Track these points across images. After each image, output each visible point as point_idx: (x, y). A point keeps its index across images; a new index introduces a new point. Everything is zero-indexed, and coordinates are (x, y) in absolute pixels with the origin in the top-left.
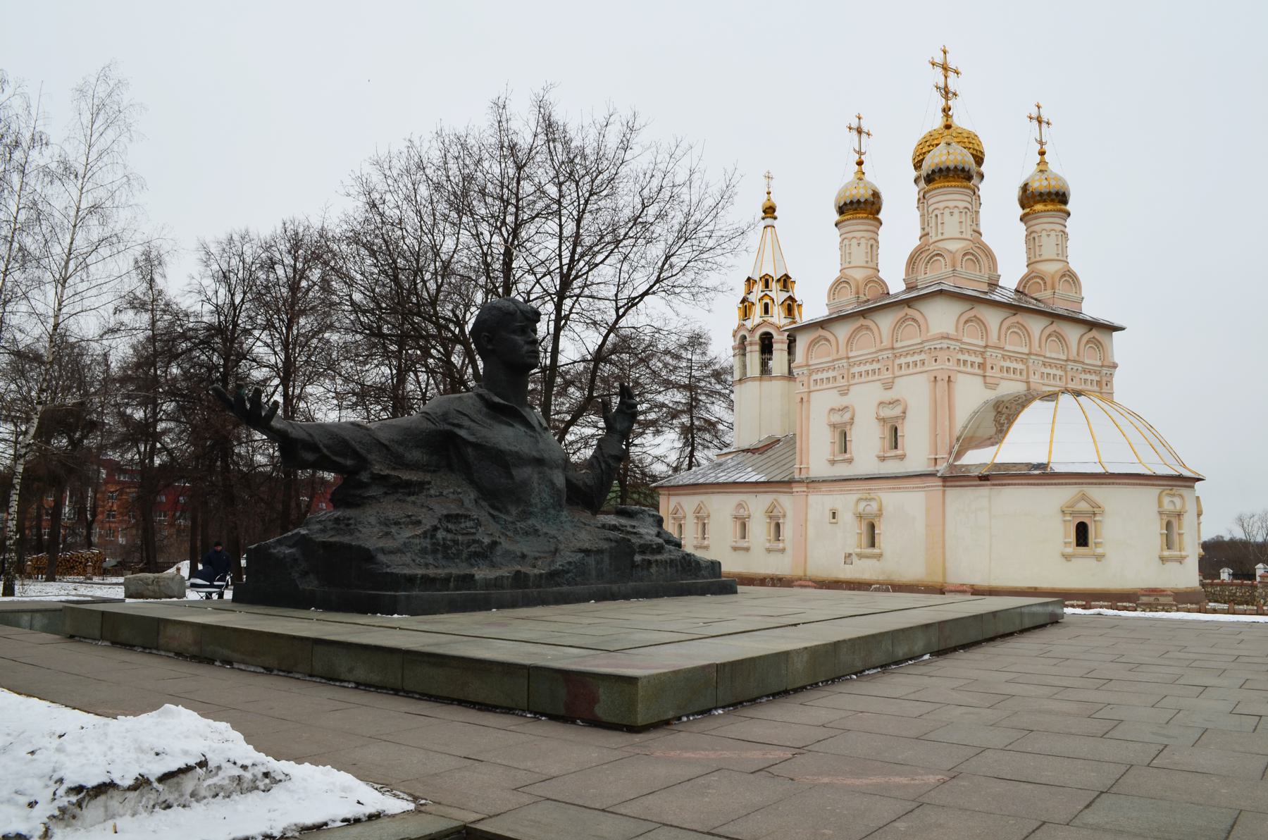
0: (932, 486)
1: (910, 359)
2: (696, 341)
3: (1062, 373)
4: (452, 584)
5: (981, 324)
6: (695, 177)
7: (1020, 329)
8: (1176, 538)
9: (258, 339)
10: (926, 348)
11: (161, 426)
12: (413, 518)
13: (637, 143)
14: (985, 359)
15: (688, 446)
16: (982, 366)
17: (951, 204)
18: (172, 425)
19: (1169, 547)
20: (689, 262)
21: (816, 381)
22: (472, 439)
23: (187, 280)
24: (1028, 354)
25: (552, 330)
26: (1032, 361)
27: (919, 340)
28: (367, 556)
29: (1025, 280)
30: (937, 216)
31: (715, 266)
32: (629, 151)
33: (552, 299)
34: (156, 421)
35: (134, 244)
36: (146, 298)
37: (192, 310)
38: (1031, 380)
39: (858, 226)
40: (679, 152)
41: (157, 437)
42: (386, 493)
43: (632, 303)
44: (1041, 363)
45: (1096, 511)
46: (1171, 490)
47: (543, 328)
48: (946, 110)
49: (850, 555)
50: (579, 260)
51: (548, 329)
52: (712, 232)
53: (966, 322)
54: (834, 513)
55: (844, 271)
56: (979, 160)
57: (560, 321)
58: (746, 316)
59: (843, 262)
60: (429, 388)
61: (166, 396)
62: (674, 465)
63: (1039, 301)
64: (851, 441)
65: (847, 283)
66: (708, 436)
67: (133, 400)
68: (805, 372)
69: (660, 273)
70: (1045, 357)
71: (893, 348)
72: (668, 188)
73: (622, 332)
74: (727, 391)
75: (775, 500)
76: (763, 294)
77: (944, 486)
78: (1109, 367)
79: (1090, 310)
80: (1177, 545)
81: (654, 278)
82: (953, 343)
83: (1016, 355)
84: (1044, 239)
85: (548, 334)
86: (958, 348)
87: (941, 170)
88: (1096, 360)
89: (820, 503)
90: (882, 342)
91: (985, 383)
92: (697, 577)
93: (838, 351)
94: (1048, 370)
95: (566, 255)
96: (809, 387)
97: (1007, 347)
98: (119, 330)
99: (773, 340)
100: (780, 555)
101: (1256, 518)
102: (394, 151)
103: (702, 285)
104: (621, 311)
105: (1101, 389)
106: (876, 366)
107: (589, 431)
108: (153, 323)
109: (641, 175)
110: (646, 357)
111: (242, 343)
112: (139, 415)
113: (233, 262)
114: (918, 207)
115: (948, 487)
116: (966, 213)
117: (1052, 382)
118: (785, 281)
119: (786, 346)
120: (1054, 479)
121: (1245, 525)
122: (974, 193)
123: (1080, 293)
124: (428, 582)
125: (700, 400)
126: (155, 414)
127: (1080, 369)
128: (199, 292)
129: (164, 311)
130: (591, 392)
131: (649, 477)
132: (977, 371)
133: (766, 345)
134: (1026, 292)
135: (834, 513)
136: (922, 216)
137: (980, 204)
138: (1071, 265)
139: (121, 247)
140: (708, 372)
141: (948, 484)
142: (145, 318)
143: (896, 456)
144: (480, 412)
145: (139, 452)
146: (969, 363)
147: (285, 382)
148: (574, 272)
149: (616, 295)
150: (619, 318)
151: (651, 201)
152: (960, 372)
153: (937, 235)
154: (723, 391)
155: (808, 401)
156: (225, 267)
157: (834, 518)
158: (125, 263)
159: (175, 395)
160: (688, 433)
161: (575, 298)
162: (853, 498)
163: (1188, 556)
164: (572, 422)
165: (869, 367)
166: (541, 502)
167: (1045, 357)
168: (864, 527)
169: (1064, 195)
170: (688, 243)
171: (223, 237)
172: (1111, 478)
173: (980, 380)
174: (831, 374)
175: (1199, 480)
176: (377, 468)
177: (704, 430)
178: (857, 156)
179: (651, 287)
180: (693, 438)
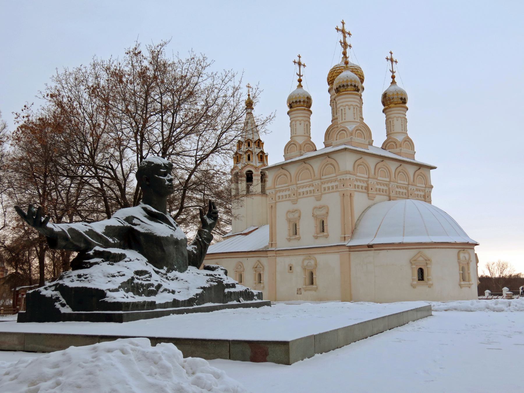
0: (343, 252)
1: (330, 185)
4: (145, 307)
7: (385, 169)
8: (467, 275)
10: (338, 179)
12: (121, 273)
16: (367, 188)
17: (349, 103)
19: (464, 280)
20: (235, 137)
21: (279, 197)
22: (142, 231)
24: (389, 182)
26: (391, 185)
27: (334, 175)
28: (101, 294)
30: (342, 110)
32: (200, 78)
38: (391, 195)
39: (300, 114)
40: (227, 79)
42: (103, 261)
44: (396, 186)
45: (428, 261)
46: (464, 250)
48: (344, 54)
49: (300, 289)
53: (358, 165)
54: (291, 267)
55: (293, 138)
56: (362, 81)
58: (238, 161)
59: (292, 133)
64: (299, 228)
65: (295, 144)
68: (273, 192)
71: (321, 179)
75: (258, 261)
76: (247, 149)
77: (350, 251)
79: (419, 158)
80: (467, 279)
82: (352, 176)
83: (383, 182)
84: (395, 122)
87: (343, 86)
88: (423, 184)
89: (283, 262)
90: (315, 176)
91: (368, 196)
92: (252, 300)
93: (291, 181)
96: (275, 200)
97: (379, 178)
99: (253, 175)
100: (457, 276)
101: (495, 265)
104: (198, 162)
105: (425, 199)
106: (311, 188)
114: (330, 105)
115: (351, 251)
116: (357, 109)
118: (258, 142)
119: (260, 178)
121: (490, 268)
123: (414, 150)
124: (136, 306)
127: (415, 189)
133: (249, 177)
135: (291, 267)
136: (333, 109)
137: (363, 103)
141: (351, 250)
143: (324, 236)
144: (145, 216)
153: (342, 120)
155: (275, 207)
157: (291, 269)
162: (301, 258)
163: (473, 284)
165: (308, 189)
166: (178, 263)
167: (398, 183)
168: (308, 274)
169: (405, 99)
172: (434, 245)
173: (365, 195)
174: (287, 193)
175: (477, 245)
176: (97, 248)
178: (298, 77)
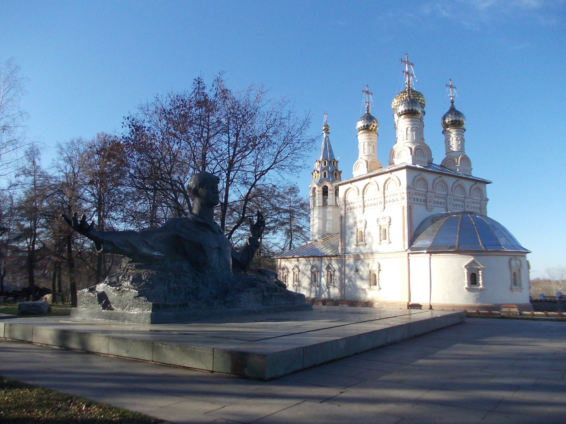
2: (293, 190)
3: (463, 204)
5: (425, 182)
6: (291, 114)
7: (443, 183)
9: (86, 189)
11: (38, 230)
13: (264, 99)
14: (426, 197)
15: (289, 238)
16: (425, 201)
18: (44, 229)
20: (289, 154)
23: (51, 162)
25: (225, 187)
29: (444, 161)
31: (301, 156)
33: (225, 172)
34: (36, 228)
35: (24, 144)
36: (31, 169)
37: (54, 175)
41: (36, 235)
43: (263, 173)
47: (221, 185)
50: (237, 154)
51: (223, 186)
52: (299, 140)
53: (417, 181)
57: (229, 182)
60: (168, 212)
61: (41, 215)
62: (282, 248)
63: (451, 170)
66: (298, 234)
67: (25, 217)
69: (275, 160)
70: (455, 196)
72: (278, 120)
73: (258, 187)
74: (307, 213)
78: (485, 200)
79: (476, 173)
81: (272, 162)
82: (412, 190)
85: (223, 188)
86: (414, 193)
91: (427, 208)
94: (456, 202)
95: (232, 151)
98: (17, 185)
102: (149, 102)
103: (295, 165)
104: (257, 177)
105: (481, 211)
107: (242, 232)
108: (35, 181)
109: (266, 114)
110: (269, 198)
111: (77, 191)
112: (27, 225)
113: (74, 153)
116: (417, 130)
117: (458, 208)
120: (499, 253)
122: (421, 121)
125: (294, 217)
126: (35, 224)
128: (58, 167)
129: (40, 176)
130: (243, 215)
131: (271, 253)
132: (423, 203)
134: (445, 166)
138: (466, 153)
139: (18, 145)
140: (298, 204)
142: (31, 178)
145: (27, 242)
146: (419, 200)
147: (99, 210)
148: (235, 159)
149: (255, 170)
150: (256, 180)
151: (271, 126)
152: (415, 204)
154: (305, 213)
156: (70, 155)
158: (21, 153)
159: (45, 215)
160: (289, 233)
161: (236, 171)
164: (236, 228)
170: (288, 145)
171: (68, 140)
173: (424, 207)
177: (296, 231)
179: (271, 166)
180: (291, 235)
